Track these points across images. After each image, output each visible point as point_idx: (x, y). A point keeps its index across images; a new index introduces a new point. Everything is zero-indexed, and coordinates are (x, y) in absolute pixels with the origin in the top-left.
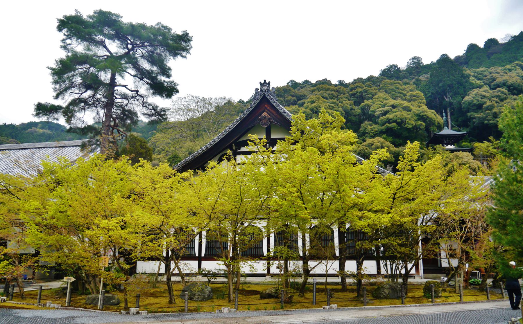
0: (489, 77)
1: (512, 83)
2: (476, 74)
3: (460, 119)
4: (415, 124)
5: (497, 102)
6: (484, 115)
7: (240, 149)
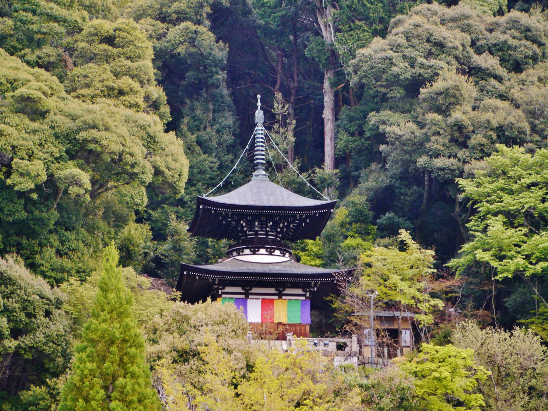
6: (419, 133)
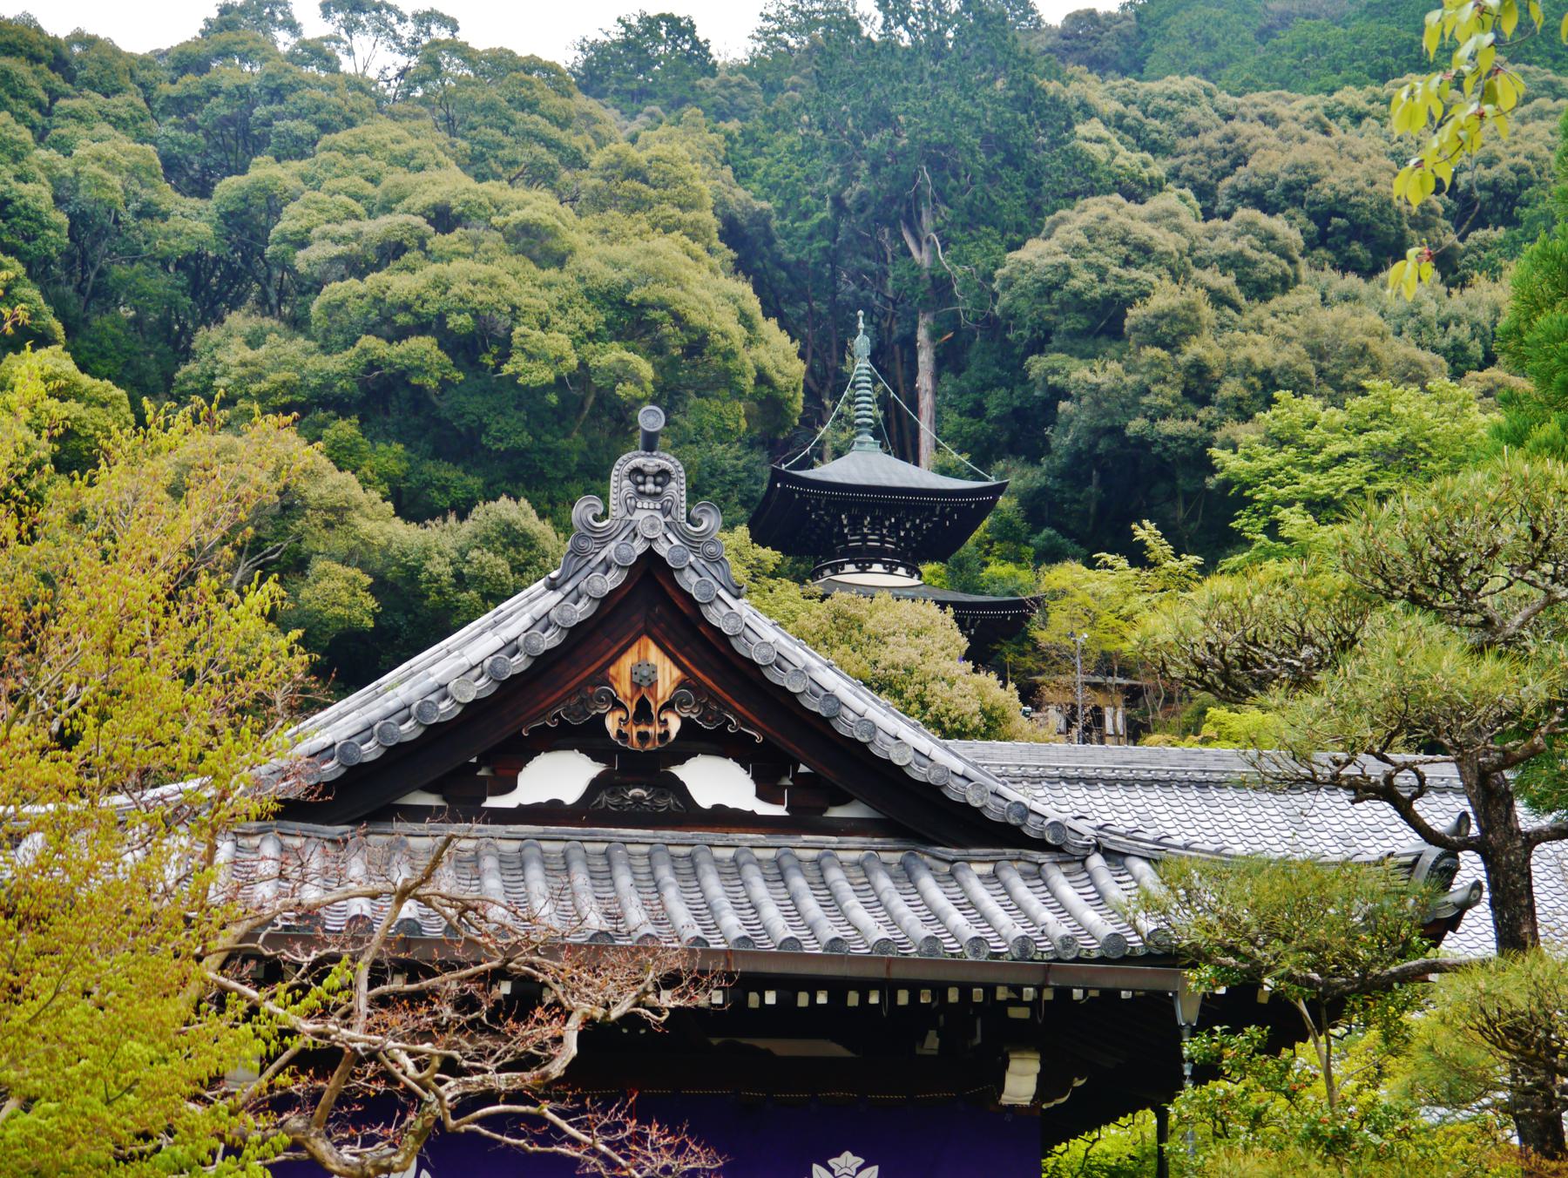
0: (1210, 140)
1: (1345, 189)
2: (1134, 112)
3: (995, 403)
4: (573, 362)
5: (1219, 299)
6: (1130, 380)
7: (509, 786)
